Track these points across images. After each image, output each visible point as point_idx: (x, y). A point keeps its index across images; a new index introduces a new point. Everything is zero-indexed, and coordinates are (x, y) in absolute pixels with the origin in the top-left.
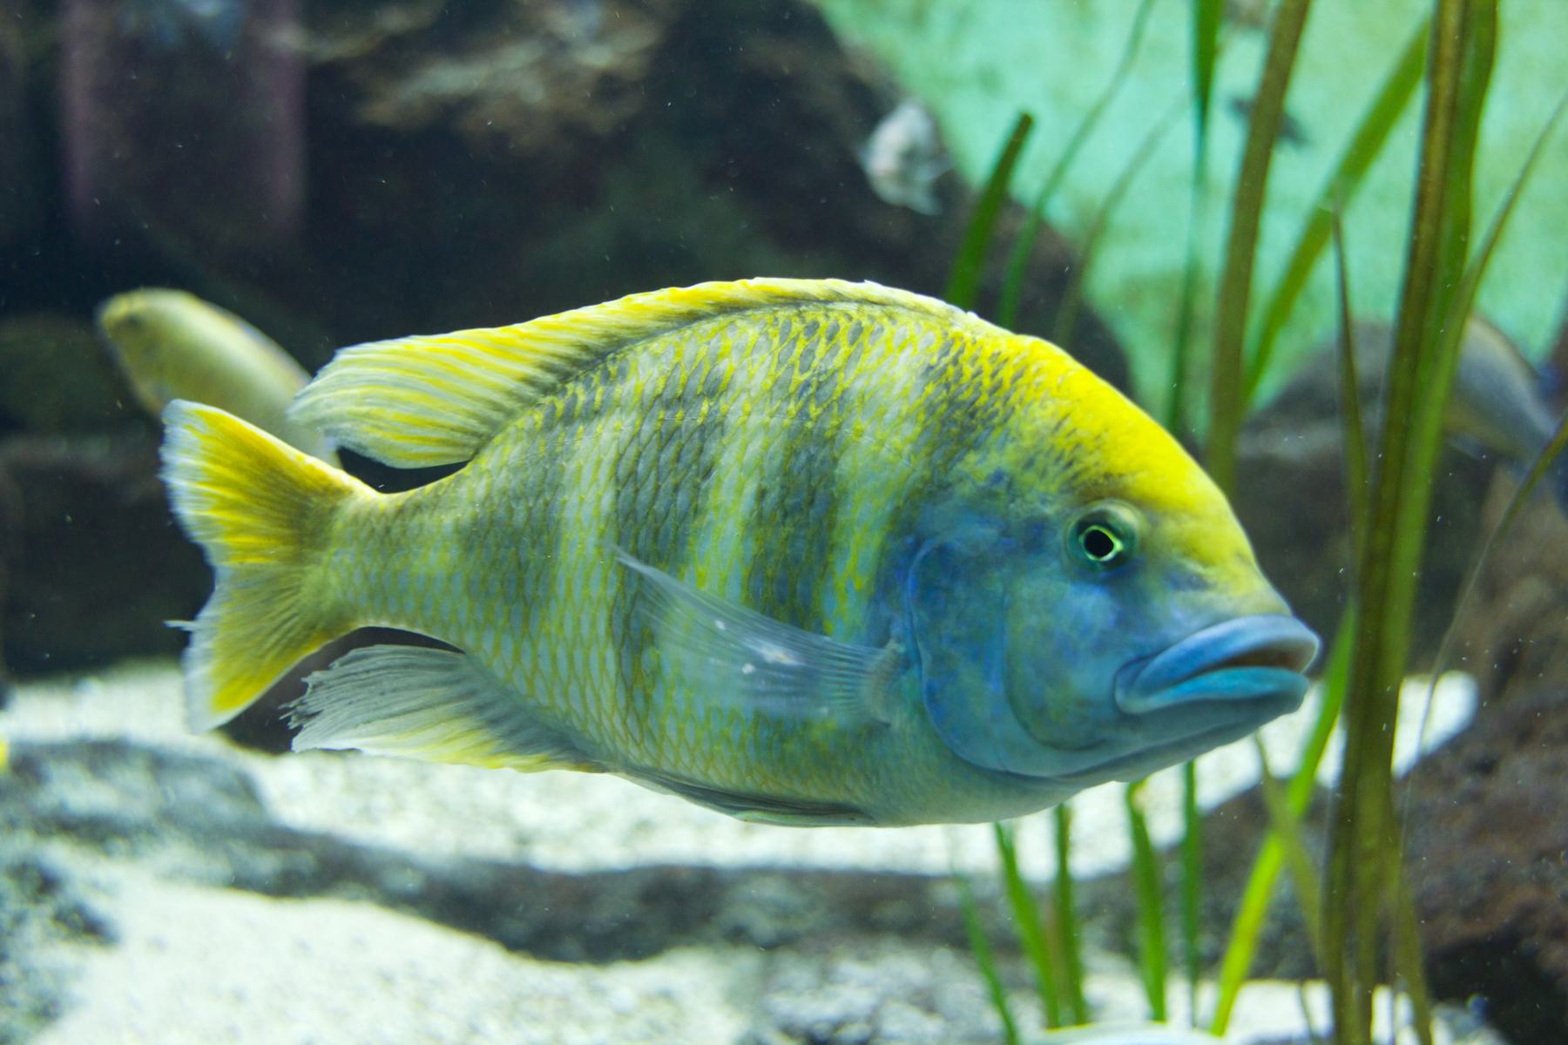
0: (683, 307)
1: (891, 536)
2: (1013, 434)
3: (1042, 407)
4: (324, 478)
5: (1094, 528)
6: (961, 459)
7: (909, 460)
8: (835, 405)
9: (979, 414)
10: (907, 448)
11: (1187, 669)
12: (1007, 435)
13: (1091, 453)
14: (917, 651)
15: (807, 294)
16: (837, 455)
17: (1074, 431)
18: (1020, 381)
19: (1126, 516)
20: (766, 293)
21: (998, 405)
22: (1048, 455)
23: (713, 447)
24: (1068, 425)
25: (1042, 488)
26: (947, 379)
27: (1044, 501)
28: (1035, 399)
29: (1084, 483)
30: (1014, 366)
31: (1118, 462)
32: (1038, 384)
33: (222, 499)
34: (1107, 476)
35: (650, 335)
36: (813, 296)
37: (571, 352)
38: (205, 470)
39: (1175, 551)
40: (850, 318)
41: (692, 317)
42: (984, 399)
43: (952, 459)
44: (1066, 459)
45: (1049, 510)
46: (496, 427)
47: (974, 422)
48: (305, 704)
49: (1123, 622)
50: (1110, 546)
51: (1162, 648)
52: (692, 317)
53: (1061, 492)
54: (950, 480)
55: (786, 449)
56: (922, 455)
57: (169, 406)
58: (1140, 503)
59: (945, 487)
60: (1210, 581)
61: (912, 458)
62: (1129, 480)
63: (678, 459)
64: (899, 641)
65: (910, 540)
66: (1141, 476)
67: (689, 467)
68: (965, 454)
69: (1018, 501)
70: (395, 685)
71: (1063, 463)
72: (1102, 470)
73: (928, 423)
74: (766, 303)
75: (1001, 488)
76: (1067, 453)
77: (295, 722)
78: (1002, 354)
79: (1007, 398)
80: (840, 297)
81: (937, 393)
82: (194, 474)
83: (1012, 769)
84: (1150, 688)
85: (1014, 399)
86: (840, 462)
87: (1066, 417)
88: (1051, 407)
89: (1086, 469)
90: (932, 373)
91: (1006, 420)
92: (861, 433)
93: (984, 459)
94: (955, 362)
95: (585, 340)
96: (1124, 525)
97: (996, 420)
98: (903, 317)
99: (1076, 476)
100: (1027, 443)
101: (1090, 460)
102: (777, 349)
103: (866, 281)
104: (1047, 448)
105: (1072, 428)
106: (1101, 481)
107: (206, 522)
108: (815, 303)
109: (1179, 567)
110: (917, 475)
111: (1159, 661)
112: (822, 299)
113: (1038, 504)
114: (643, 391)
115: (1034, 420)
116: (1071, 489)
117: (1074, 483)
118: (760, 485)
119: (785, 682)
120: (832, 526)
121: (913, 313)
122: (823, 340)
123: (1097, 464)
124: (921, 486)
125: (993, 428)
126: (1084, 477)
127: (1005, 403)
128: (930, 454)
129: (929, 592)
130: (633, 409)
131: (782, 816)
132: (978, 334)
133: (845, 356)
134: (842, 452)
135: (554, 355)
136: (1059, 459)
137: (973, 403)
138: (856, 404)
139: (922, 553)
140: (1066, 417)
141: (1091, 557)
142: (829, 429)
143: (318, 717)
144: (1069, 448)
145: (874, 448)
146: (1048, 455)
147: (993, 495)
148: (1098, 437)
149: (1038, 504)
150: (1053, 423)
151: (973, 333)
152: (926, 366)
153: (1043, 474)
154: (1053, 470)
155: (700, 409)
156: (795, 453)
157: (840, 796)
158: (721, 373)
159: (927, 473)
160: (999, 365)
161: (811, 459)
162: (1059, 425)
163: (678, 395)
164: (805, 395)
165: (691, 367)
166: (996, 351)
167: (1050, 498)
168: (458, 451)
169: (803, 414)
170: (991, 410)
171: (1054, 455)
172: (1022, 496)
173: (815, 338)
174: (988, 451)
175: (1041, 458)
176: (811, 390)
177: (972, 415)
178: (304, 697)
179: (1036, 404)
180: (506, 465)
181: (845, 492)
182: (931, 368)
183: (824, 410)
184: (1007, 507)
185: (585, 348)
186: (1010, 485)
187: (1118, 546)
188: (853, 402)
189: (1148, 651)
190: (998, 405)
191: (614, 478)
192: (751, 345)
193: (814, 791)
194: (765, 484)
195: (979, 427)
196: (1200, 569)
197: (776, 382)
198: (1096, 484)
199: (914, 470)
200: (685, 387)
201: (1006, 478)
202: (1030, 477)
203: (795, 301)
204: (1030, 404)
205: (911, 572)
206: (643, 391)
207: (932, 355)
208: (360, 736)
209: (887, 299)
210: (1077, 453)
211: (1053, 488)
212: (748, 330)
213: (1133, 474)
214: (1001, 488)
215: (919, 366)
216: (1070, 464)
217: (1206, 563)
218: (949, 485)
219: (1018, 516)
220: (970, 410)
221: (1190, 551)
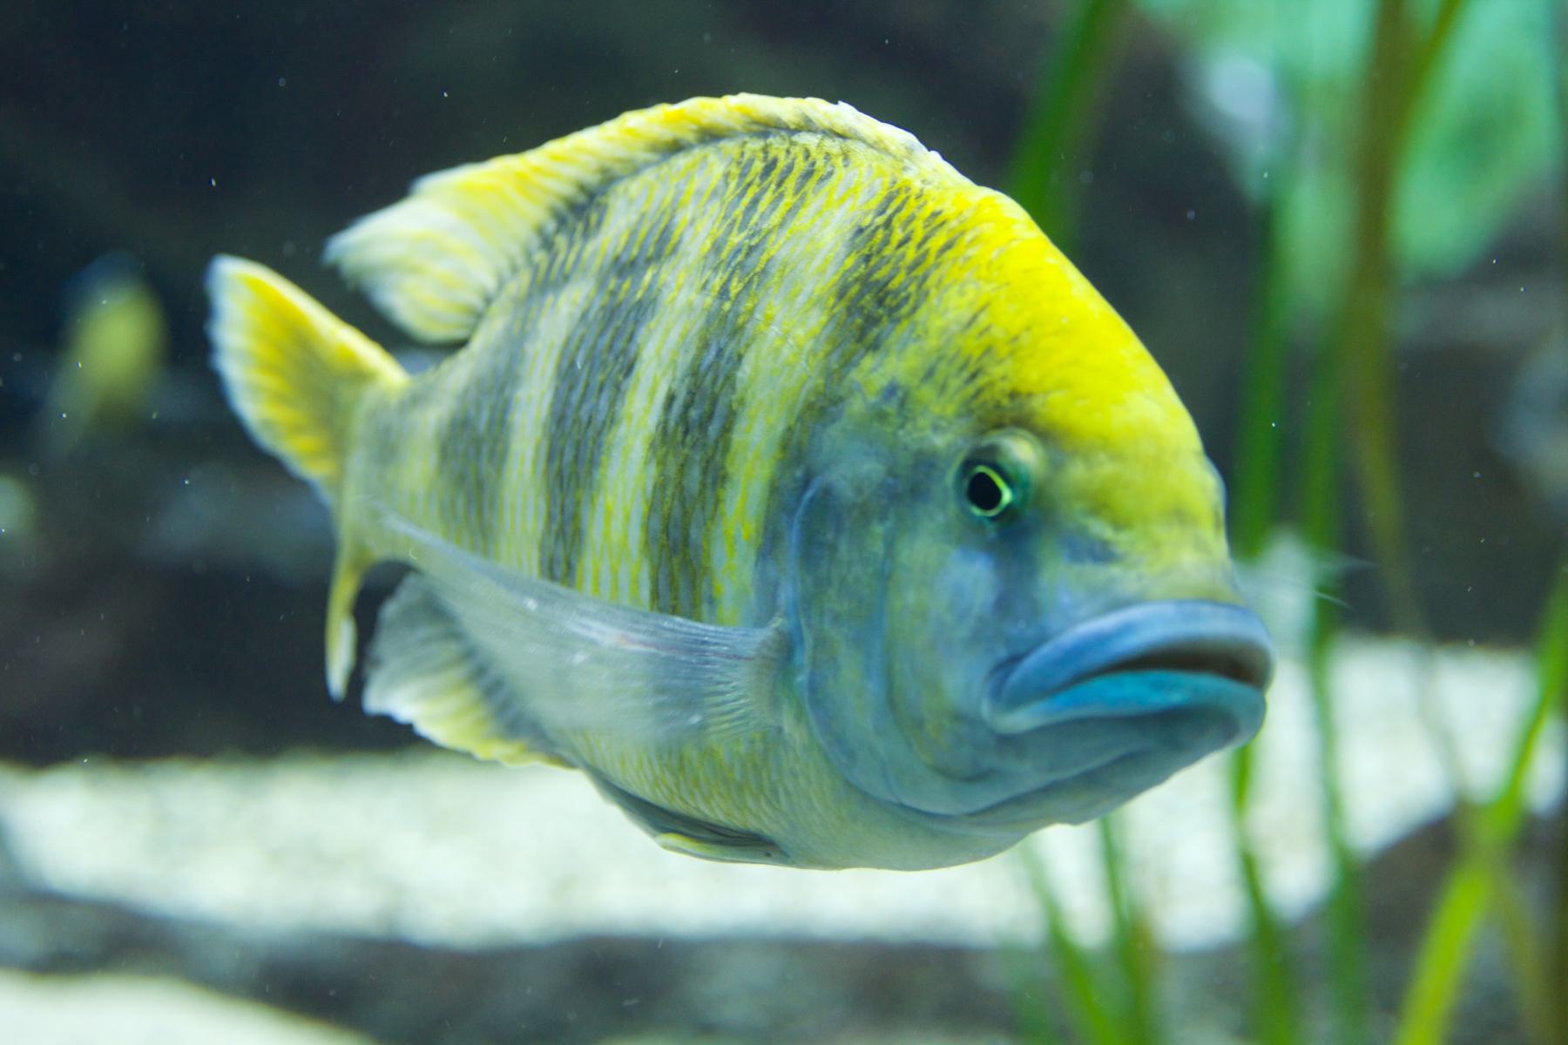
0: (667, 135)
2: (919, 330)
3: (962, 293)
5: (981, 469)
6: (856, 365)
7: (807, 361)
8: (756, 279)
9: (888, 301)
10: (809, 345)
11: (1063, 675)
12: (912, 331)
13: (1000, 362)
14: (799, 628)
15: (779, 119)
16: (742, 352)
17: (987, 329)
18: (950, 254)
19: (1022, 451)
20: (745, 115)
21: (912, 288)
22: (951, 362)
24: (984, 320)
26: (871, 248)
27: (936, 428)
28: (955, 281)
29: (984, 403)
30: (950, 230)
31: (1030, 374)
32: (967, 259)
34: (1013, 395)
35: (635, 170)
36: (785, 123)
39: (1078, 506)
41: (676, 148)
42: (901, 277)
43: (848, 363)
44: (971, 369)
45: (940, 441)
46: (488, 301)
47: (881, 311)
49: (1004, 605)
50: (997, 494)
51: (1042, 639)
52: (676, 148)
53: (959, 415)
54: (842, 392)
55: (700, 339)
56: (821, 355)
58: (1046, 435)
59: (838, 401)
60: (1120, 550)
61: (811, 358)
62: (1036, 403)
63: (611, 347)
64: (786, 615)
65: (799, 473)
66: (1056, 398)
68: (862, 357)
69: (909, 426)
71: (965, 374)
72: (1006, 386)
73: (835, 310)
75: (891, 408)
78: (944, 214)
79: (925, 278)
80: (807, 126)
81: (855, 268)
83: (907, 802)
84: (1016, 700)
85: (931, 281)
87: (983, 309)
88: (971, 292)
89: (991, 384)
91: (914, 310)
92: (769, 321)
93: (880, 364)
94: (888, 224)
96: (1016, 465)
98: (859, 151)
99: (979, 392)
100: (932, 343)
101: (997, 371)
102: (728, 197)
103: (841, 103)
104: (951, 352)
106: (1005, 402)
107: (268, 424)
108: (783, 133)
109: (1083, 530)
110: (810, 385)
111: (1030, 663)
115: (946, 311)
116: (970, 412)
118: (670, 389)
120: (727, 449)
121: (870, 150)
122: (773, 187)
123: (1004, 378)
124: (812, 399)
125: (898, 321)
126: (986, 396)
127: (920, 287)
128: (828, 355)
129: (813, 550)
131: (706, 845)
132: (930, 183)
133: (787, 208)
134: (748, 346)
136: (963, 367)
137: (886, 284)
139: (809, 495)
141: (977, 511)
142: (744, 313)
144: (977, 353)
145: (778, 343)
146: (951, 362)
147: (882, 416)
148: (1015, 339)
149: (928, 432)
151: (923, 181)
152: (855, 229)
153: (943, 388)
154: (955, 383)
156: (706, 346)
157: (752, 824)
161: (720, 352)
163: (632, 258)
164: (733, 264)
166: (938, 208)
167: (944, 424)
170: (903, 294)
171: (959, 362)
172: (914, 419)
173: (766, 182)
174: (887, 352)
175: (942, 366)
176: (740, 258)
177: (880, 302)
179: (955, 288)
182: (860, 231)
184: (894, 434)
185: (582, 188)
186: (903, 403)
187: (1007, 496)
190: (912, 288)
192: (710, 189)
193: (718, 811)
194: (674, 386)
195: (885, 319)
196: (1107, 532)
198: (998, 406)
201: (900, 394)
202: (927, 393)
203: (766, 128)
204: (948, 287)
205: (796, 521)
207: (866, 214)
209: (850, 129)
211: (950, 410)
212: (714, 165)
213: (1046, 393)
214: (891, 408)
215: (848, 229)
217: (1119, 525)
218: (841, 399)
219: (906, 448)
220: (881, 294)
221: (1099, 506)
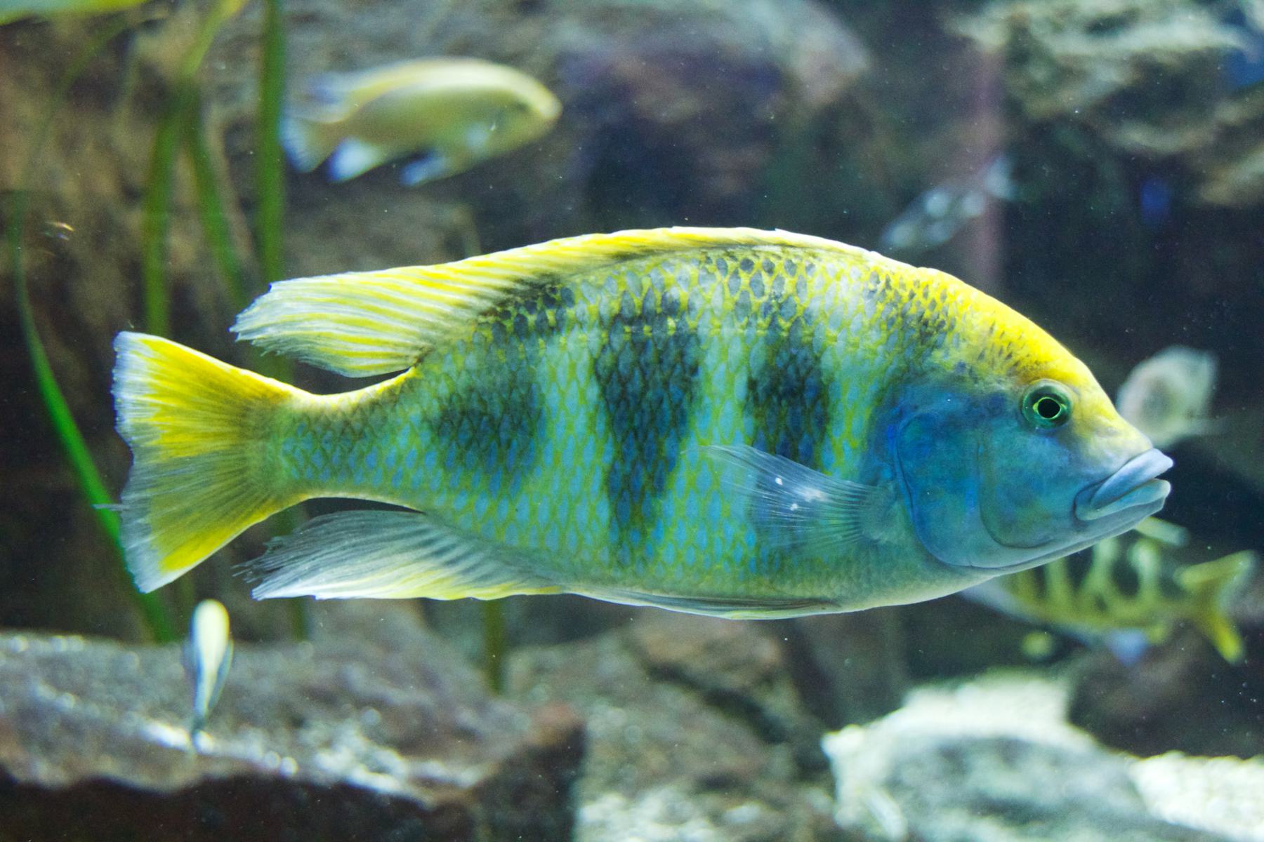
1: (877, 410)
4: (262, 386)
23: (692, 352)
24: (996, 328)
25: (995, 373)
33: (164, 407)
37: (507, 284)
38: (151, 384)
40: (779, 258)
48: (263, 562)
50: (1040, 408)
51: (1107, 478)
52: (623, 257)
57: (118, 337)
61: (887, 356)
67: (674, 367)
70: (354, 541)
72: (1034, 359)
74: (692, 246)
76: (1005, 348)
77: (251, 577)
82: (141, 388)
86: (822, 359)
87: (993, 325)
90: (876, 296)
95: (520, 275)
97: (946, 327)
105: (1002, 332)
111: (1107, 484)
112: (743, 243)
113: (995, 384)
114: (599, 313)
117: (1017, 369)
119: (838, 506)
125: (945, 333)
130: (593, 325)
135: (486, 286)
136: (1001, 352)
138: (820, 318)
140: (993, 325)
143: (279, 572)
144: (1005, 345)
147: (961, 379)
150: (987, 329)
153: (993, 364)
154: (999, 361)
155: (667, 325)
158: (658, 295)
159: (903, 365)
160: (925, 289)
162: (992, 329)
165: (641, 293)
168: (403, 361)
169: (773, 326)
178: (262, 557)
180: (443, 373)
181: (831, 380)
183: (793, 323)
188: (817, 317)
189: (1098, 479)
191: (594, 377)
197: (737, 304)
199: (891, 364)
200: (643, 308)
202: (984, 365)
206: (599, 313)
208: (316, 583)
210: (1012, 348)
214: (966, 375)
216: (1010, 356)
